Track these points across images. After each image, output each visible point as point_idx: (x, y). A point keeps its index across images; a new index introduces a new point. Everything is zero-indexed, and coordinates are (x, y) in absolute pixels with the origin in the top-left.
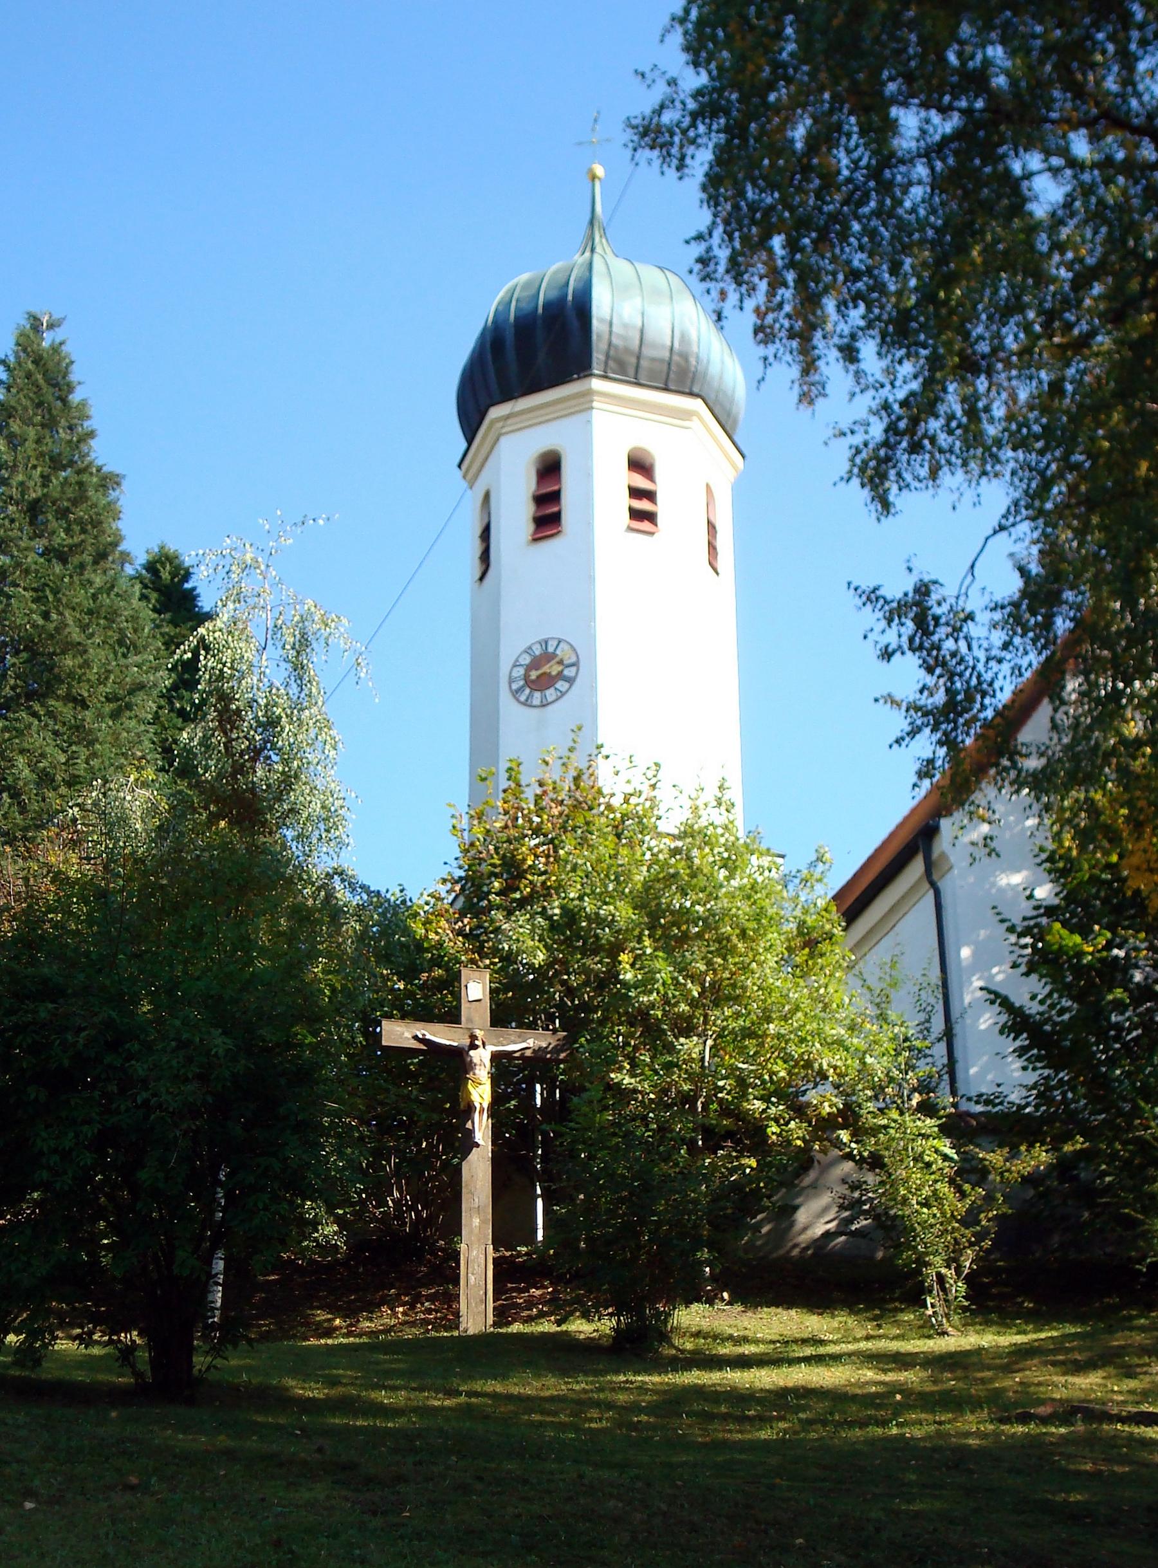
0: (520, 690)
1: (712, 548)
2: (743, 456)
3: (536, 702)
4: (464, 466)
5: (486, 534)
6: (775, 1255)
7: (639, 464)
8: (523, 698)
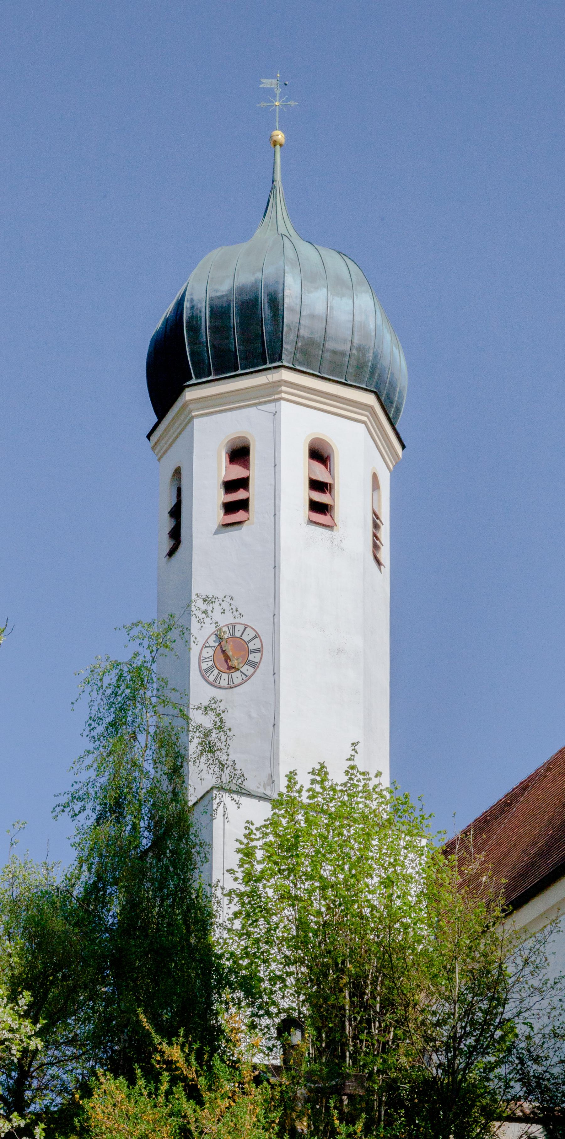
0: (209, 670)
1: (376, 547)
2: (403, 447)
3: (224, 683)
4: (154, 437)
5: (176, 512)
6: (401, 456)
7: (319, 454)
8: (211, 678)
